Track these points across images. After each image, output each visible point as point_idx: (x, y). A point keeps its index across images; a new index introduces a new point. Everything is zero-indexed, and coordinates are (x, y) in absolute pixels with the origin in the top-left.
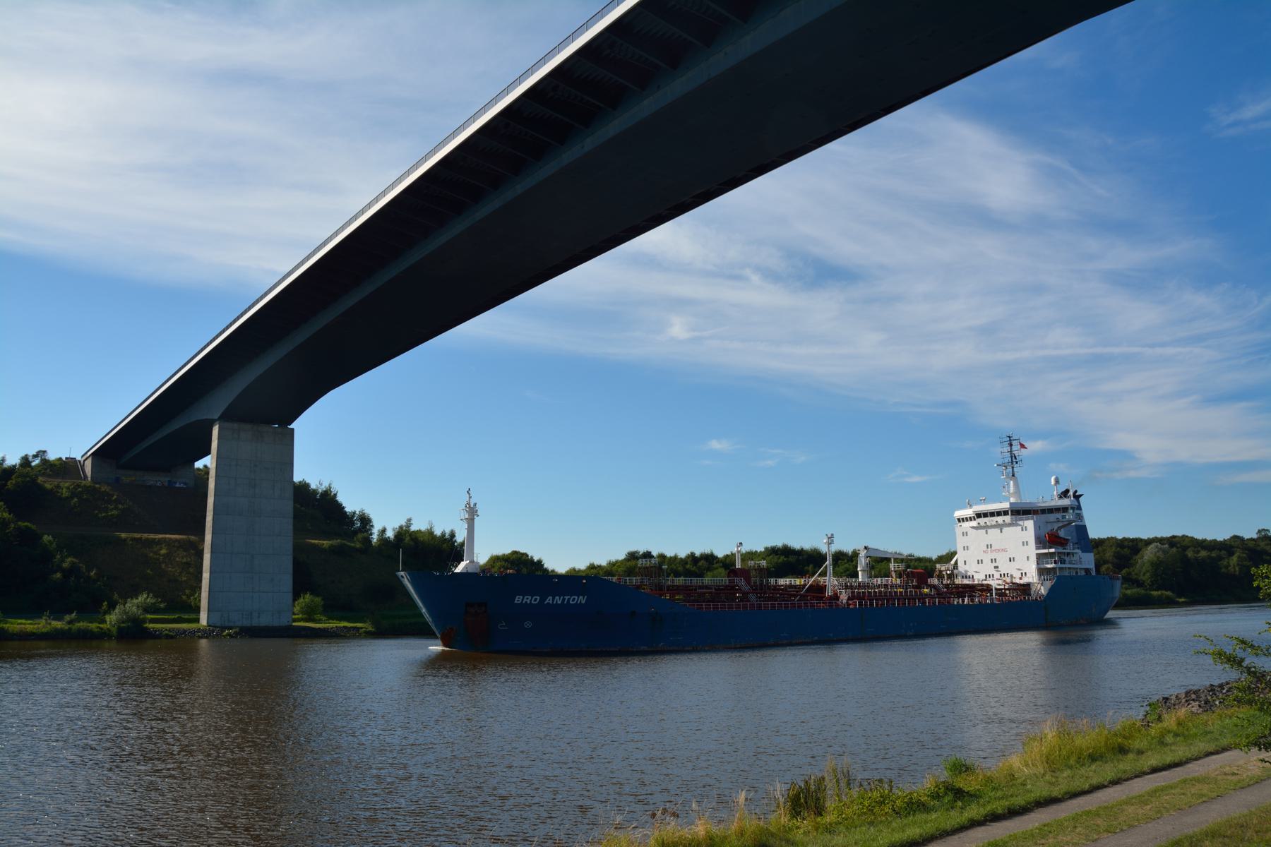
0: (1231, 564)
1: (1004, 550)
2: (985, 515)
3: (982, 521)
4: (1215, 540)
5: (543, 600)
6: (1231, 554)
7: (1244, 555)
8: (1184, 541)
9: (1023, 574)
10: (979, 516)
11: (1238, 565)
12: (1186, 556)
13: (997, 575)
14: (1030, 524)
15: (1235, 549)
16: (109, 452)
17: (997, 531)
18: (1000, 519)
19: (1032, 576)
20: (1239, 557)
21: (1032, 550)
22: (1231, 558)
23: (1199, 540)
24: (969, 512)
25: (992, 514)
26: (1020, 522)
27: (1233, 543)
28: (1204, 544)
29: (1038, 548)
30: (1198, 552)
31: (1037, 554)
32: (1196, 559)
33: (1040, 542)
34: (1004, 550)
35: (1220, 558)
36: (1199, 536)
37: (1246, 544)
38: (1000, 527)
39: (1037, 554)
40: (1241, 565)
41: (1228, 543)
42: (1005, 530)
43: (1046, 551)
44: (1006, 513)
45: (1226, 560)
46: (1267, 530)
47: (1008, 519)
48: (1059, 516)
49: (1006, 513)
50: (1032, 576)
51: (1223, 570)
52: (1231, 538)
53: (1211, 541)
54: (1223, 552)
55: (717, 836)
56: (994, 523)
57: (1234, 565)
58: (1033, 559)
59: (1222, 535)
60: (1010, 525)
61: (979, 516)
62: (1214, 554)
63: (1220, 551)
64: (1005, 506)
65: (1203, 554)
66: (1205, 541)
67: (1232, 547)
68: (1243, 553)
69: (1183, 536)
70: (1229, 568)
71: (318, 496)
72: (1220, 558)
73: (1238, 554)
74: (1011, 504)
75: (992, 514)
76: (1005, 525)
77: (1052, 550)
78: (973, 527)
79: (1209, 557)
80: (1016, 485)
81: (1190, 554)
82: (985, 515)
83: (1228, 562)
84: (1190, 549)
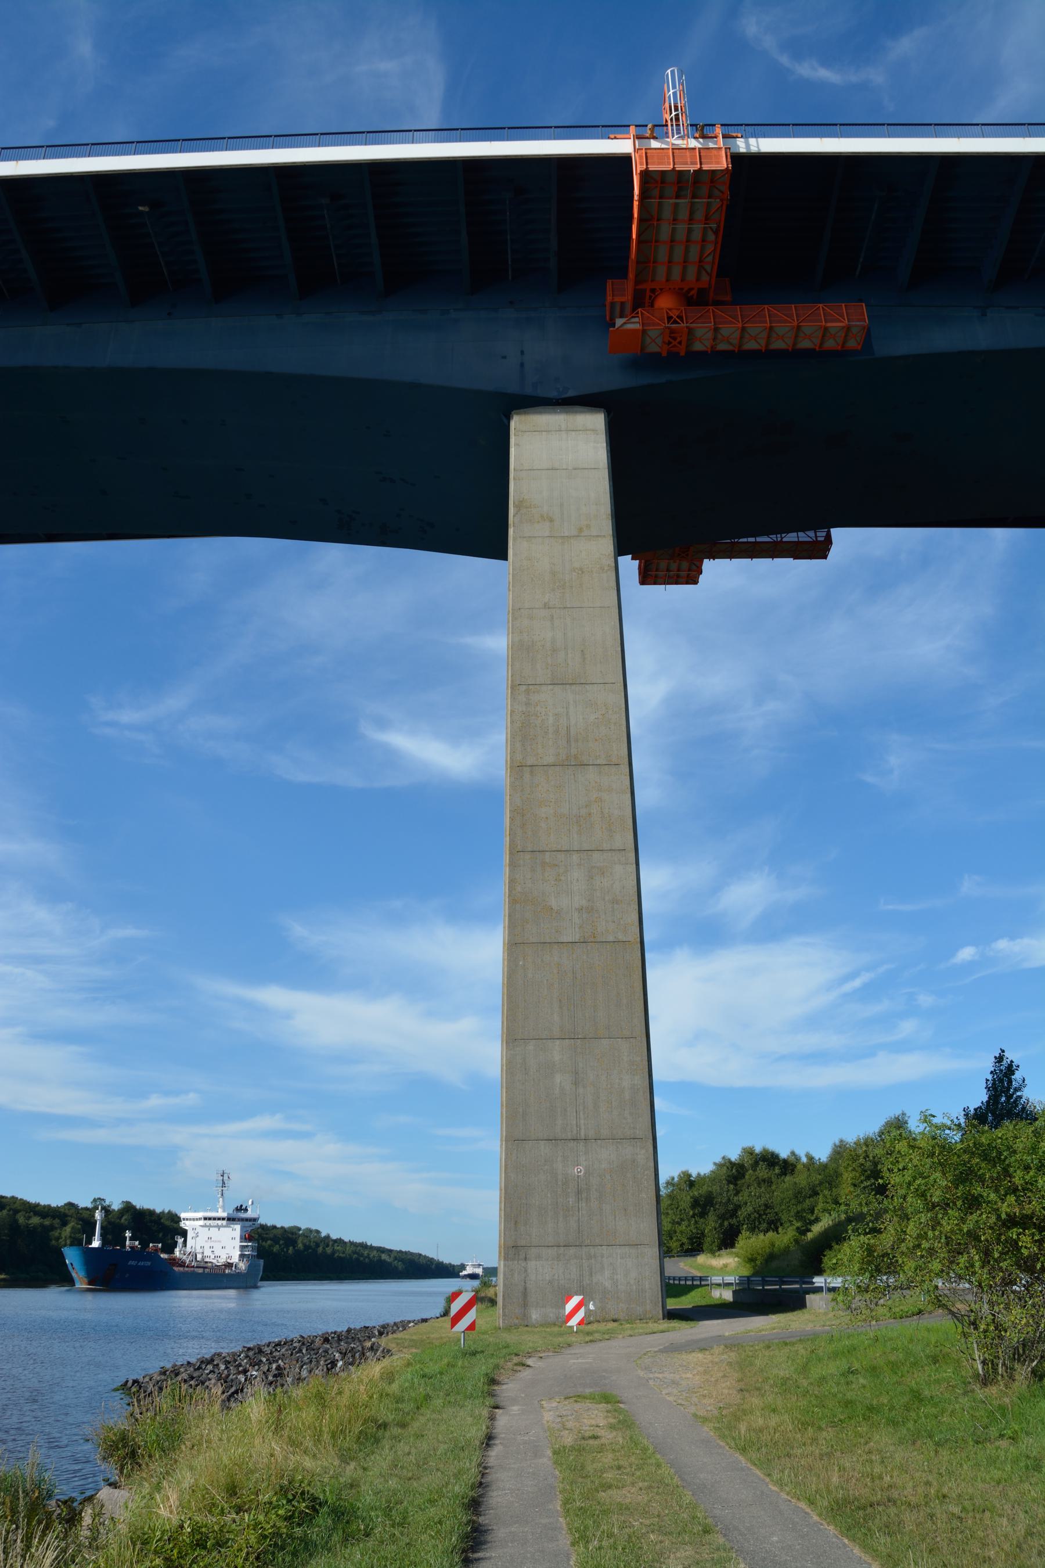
0: (63, 1236)
1: (220, 1241)
2: (210, 1219)
3: (208, 1222)
4: (49, 1206)
5: (763, 1287)
6: (64, 1224)
7: (79, 1226)
8: (14, 1203)
9: (230, 1257)
10: (205, 1219)
11: (70, 1237)
12: (16, 1221)
13: (212, 1256)
14: (238, 1227)
15: (69, 1218)
16: (572, 1297)
17: (217, 1229)
18: (220, 1222)
19: (235, 1259)
20: (73, 1228)
21: (237, 1243)
22: (64, 1228)
23: (32, 1203)
24: (200, 1215)
25: (214, 1219)
26: (232, 1226)
27: (67, 1211)
28: (37, 1209)
29: (241, 1242)
30: (29, 1218)
31: (240, 1246)
32: (27, 1225)
33: (243, 1238)
34: (220, 1241)
35: (52, 1228)
36: (32, 1199)
37: (81, 1214)
38: (219, 1227)
39: (240, 1246)
40: (74, 1238)
41: (62, 1210)
42: (221, 1229)
43: (246, 1244)
44: (223, 1219)
45: (59, 1231)
46: (103, 1200)
47: (224, 1222)
48: (251, 1223)
49: (223, 1219)
50: (235, 1259)
51: (54, 1242)
52: (66, 1205)
53: (45, 1206)
54: (57, 1221)
55: (701, 1196)
56: (216, 1224)
57: (66, 1237)
58: (238, 1248)
59: (56, 1201)
60: (225, 1227)
61: (205, 1219)
62: (47, 1222)
63: (54, 1219)
64: (225, 1215)
65: (35, 1220)
66: (38, 1205)
67: (65, 1215)
68: (77, 1224)
69: (13, 1197)
70: (61, 1240)
71: (433, 1266)
72: (52, 1228)
73: (73, 1224)
74: (228, 1214)
75: (214, 1219)
76: (222, 1226)
77: (250, 1244)
78: (201, 1226)
79: (42, 1225)
80: (223, 1201)
81: (21, 1219)
82: (210, 1219)
83: (60, 1233)
84: (20, 1213)
